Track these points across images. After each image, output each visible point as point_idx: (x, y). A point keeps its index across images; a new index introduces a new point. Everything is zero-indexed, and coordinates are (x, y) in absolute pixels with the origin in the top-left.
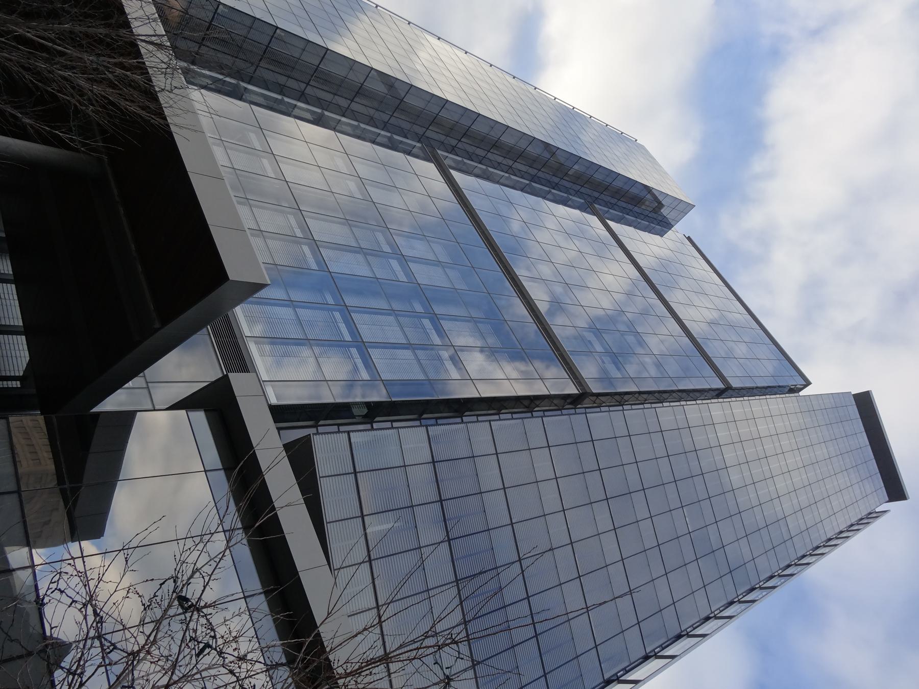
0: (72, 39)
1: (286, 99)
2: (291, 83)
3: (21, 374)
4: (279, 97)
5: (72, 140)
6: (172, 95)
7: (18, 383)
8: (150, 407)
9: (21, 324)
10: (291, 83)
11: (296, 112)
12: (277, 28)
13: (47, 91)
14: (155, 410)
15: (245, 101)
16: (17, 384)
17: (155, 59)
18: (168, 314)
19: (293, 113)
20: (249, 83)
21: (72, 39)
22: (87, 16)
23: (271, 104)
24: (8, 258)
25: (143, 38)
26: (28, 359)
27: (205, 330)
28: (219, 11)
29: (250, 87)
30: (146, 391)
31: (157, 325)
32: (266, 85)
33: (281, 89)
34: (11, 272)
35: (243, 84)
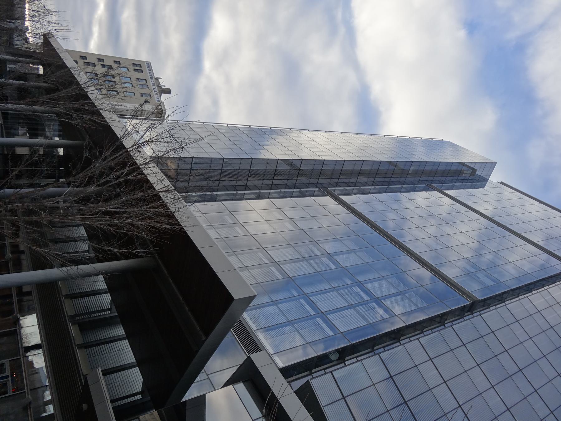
1: (239, 192)
2: (239, 183)
4: (235, 192)
5: (138, 252)
10: (239, 183)
15: (218, 201)
16: (139, 397)
20: (218, 191)
21: (128, 203)
22: (132, 190)
26: (142, 380)
28: (193, 162)
29: (219, 193)
30: (208, 380)
31: (204, 338)
35: (215, 193)
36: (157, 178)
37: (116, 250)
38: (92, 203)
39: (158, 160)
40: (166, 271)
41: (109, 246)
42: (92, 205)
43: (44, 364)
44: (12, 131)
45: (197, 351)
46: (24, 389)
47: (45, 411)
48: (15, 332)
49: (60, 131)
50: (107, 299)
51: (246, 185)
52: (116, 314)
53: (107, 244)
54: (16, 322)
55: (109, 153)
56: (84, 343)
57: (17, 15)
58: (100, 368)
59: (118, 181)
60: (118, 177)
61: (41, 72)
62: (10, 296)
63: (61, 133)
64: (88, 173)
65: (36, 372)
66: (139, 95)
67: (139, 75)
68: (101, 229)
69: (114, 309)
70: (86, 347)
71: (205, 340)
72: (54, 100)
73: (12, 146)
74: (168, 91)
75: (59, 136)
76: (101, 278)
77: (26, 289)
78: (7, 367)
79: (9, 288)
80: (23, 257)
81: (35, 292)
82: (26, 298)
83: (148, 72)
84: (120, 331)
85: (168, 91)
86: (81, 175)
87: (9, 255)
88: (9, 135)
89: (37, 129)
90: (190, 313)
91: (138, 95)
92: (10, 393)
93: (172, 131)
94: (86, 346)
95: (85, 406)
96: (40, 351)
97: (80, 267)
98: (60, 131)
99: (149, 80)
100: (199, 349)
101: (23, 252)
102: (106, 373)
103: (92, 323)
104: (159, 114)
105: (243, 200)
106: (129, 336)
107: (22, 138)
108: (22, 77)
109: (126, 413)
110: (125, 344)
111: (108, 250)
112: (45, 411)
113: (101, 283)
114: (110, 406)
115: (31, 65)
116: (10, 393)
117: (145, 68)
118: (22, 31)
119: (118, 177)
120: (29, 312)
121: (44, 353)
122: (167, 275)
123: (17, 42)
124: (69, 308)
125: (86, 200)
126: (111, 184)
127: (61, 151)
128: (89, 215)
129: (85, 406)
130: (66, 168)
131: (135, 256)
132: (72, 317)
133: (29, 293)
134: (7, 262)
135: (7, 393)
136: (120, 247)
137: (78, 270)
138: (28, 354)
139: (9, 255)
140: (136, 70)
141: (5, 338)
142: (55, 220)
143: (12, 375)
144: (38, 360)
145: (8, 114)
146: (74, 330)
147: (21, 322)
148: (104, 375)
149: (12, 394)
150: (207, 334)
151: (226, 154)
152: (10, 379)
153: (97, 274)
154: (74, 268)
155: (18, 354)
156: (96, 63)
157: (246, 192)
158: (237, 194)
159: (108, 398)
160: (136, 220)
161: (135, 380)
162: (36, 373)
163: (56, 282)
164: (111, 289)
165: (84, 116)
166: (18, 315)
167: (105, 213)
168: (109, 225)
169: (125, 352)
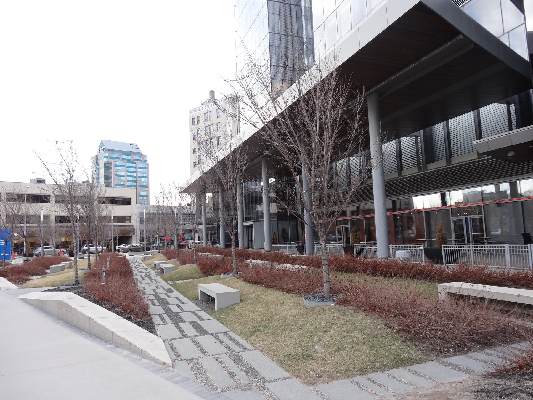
0: (312, 116)
1: (303, 13)
2: (294, 14)
3: (506, 105)
4: (303, 18)
5: (360, 104)
6: (321, 66)
7: (511, 105)
8: (523, 26)
9: (472, 112)
10: (294, 14)
11: (308, 5)
12: (269, 33)
13: (340, 121)
14: (525, 23)
15: (313, 36)
16: (512, 106)
17: (307, 83)
18: (453, 32)
19: (309, 6)
20: (302, 37)
21: (312, 116)
22: (298, 111)
23: (309, 21)
24: (434, 126)
25: (298, 86)
26: (496, 104)
27: (462, 9)
28: (274, 64)
29: (304, 36)
30: (510, 33)
31: (461, 37)
32: (300, 28)
33: (299, 18)
34: (442, 123)
35: (305, 40)
36: (289, 97)
37: (357, 125)
38: (312, 148)
39: (274, 97)
40: (383, 83)
41: (352, 131)
42: (313, 147)
43: (461, 191)
44: (259, 214)
45: (475, 44)
46: (480, 206)
47: (505, 192)
48: (428, 213)
49: (256, 181)
50: (406, 141)
51: (296, 5)
52: (422, 131)
53: (350, 133)
54: (419, 212)
55: (264, 133)
56: (446, 158)
57: (170, 211)
58: (474, 142)
59: (290, 125)
60: (287, 126)
61: (210, 195)
62: (395, 216)
63: (258, 179)
64: (284, 151)
65: (466, 199)
66: (218, 119)
67: (202, 119)
68: (335, 140)
69: (416, 134)
70: (451, 157)
71: (464, 36)
72: (227, 181)
73: (271, 215)
74: (212, 93)
75: (260, 181)
76: (384, 146)
77: (390, 205)
78: (457, 218)
79: (388, 218)
80: (362, 207)
81: (394, 198)
82: (398, 206)
83: (197, 112)
84: (439, 128)
85: (212, 93)
86: (286, 157)
87: (359, 217)
88: (262, 217)
89: (256, 197)
90: (430, 55)
91: (219, 120)
92: (482, 216)
93: (240, 76)
94: (449, 156)
95: (510, 154)
96: (447, 194)
97: (372, 155)
98: (256, 181)
99: (205, 110)
100: (472, 41)
101: (358, 207)
102: (479, 135)
103: (429, 151)
104: (234, 100)
105: (311, 8)
106: (445, 118)
107: (263, 208)
108: (216, 209)
109: (526, 116)
110: (453, 122)
111: (356, 131)
112: (505, 192)
113: (390, 146)
114: (515, 131)
115: (207, 202)
116: (482, 216)
117: (195, 115)
118: (181, 207)
119: (287, 126)
120: (410, 204)
121: (449, 191)
122: (387, 82)
123: (188, 211)
124: (411, 171)
125: (309, 154)
126: (293, 132)
127: (272, 180)
128: (323, 150)
129: (510, 154)
130: (285, 173)
131: (364, 113)
132: (420, 169)
133: (394, 202)
134: (366, 218)
135: (482, 219)
136: (354, 121)
137: (374, 157)
138: (448, 204)
139: (359, 217)
140: (198, 122)
141: (431, 221)
142: (327, 177)
143: (465, 215)
144: (456, 197)
145: (246, 217)
146: (432, 167)
147: (418, 208)
148: (481, 137)
149: (483, 215)
150: (457, 32)
151: (266, 30)
152: (469, 216)
153: (381, 149)
154: (373, 161)
155: (447, 211)
156: (197, 154)
157: (303, 5)
158: (305, 15)
159: (507, 133)
160: (329, 111)
161: (494, 112)
162: (468, 200)
163: (385, 182)
164: (397, 136)
165: (238, 158)
166: (412, 210)
167: (321, 135)
168: (333, 132)
169: (462, 123)
